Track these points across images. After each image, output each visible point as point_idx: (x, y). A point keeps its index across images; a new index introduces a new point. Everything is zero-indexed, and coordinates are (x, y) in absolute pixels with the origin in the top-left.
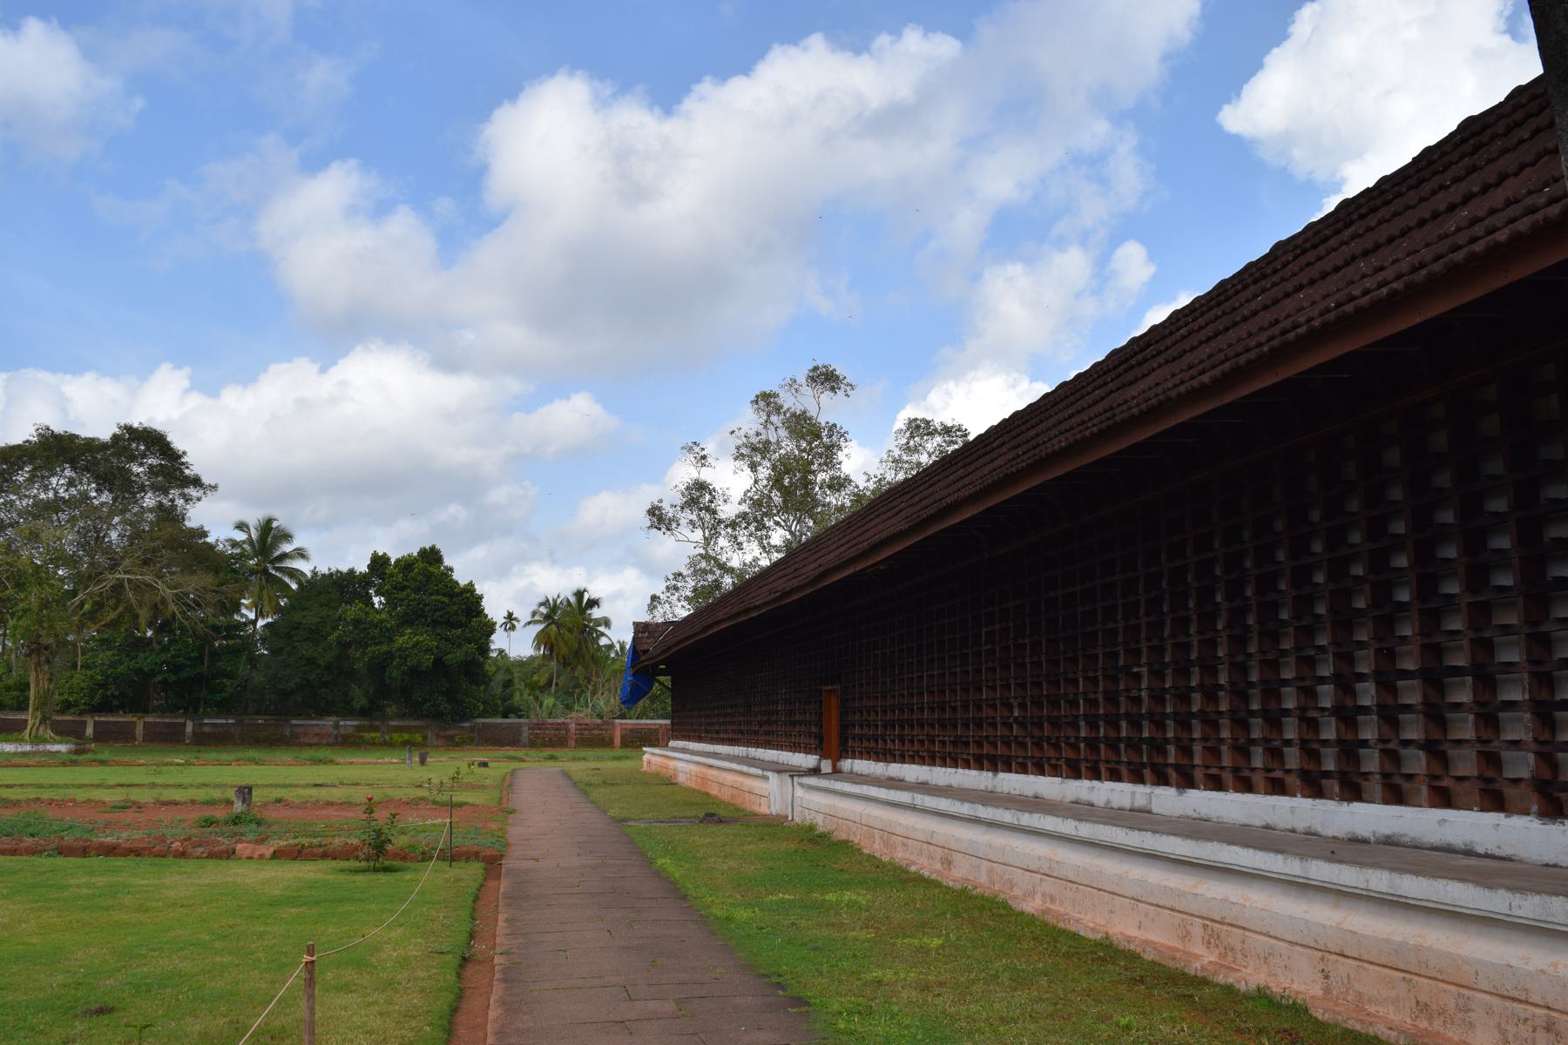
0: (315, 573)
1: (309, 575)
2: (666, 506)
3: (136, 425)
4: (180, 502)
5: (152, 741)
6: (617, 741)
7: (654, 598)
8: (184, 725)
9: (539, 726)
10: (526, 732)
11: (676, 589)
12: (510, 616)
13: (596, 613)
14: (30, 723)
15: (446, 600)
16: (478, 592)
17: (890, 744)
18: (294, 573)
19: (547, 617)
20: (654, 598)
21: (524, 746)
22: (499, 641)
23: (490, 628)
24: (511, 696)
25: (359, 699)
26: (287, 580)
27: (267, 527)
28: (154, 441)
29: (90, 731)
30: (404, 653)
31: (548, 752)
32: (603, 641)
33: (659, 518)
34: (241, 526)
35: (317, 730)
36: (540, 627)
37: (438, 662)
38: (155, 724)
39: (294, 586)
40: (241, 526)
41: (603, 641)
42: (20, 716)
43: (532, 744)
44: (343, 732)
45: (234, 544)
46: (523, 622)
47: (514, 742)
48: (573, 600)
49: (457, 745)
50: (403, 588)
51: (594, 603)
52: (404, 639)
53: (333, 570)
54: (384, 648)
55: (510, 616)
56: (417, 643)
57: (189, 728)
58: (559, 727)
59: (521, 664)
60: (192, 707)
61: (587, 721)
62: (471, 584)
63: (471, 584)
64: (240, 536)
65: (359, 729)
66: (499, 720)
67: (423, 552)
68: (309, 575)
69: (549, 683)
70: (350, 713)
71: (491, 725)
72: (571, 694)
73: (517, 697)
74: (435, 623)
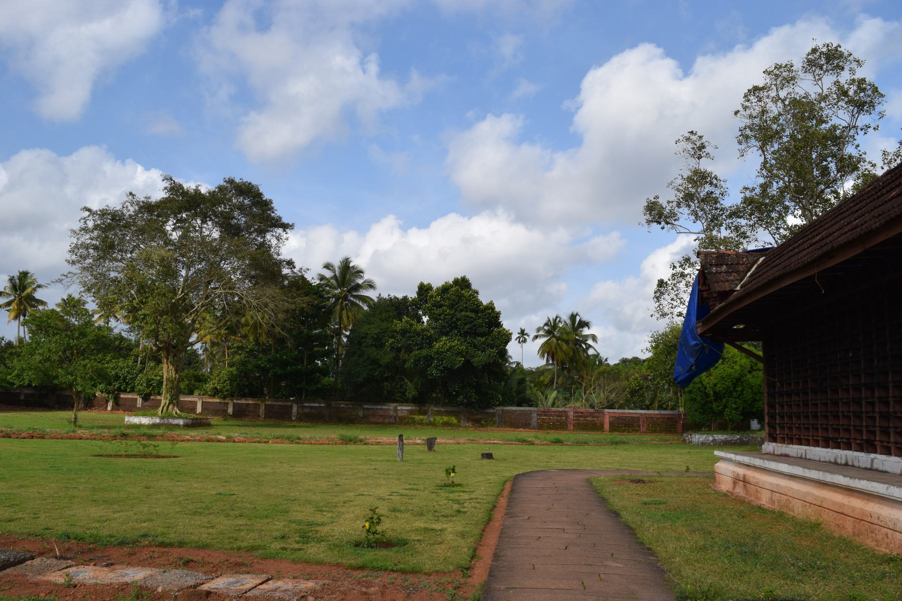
0: (380, 298)
1: (376, 300)
2: (662, 201)
3: (237, 180)
4: (274, 242)
5: (270, 417)
6: (607, 426)
7: (661, 283)
8: (291, 407)
9: (545, 413)
11: (683, 275)
12: (522, 332)
13: (586, 331)
14: (163, 402)
15: (473, 315)
16: (497, 310)
17: (794, 431)
18: (364, 299)
19: (549, 332)
20: (661, 283)
21: (534, 428)
22: (513, 349)
23: (507, 337)
24: (524, 390)
25: (411, 390)
26: (361, 304)
27: (346, 265)
28: (248, 190)
29: (230, 410)
30: (438, 358)
31: (553, 435)
32: (591, 352)
33: (657, 214)
34: (328, 266)
35: (381, 413)
36: (543, 340)
37: (468, 363)
38: (272, 406)
39: (366, 308)
40: (328, 266)
41: (591, 352)
42: (159, 397)
43: (540, 427)
44: (400, 414)
45: (322, 278)
46: (532, 336)
47: (526, 425)
49: (483, 426)
50: (441, 306)
51: (584, 324)
52: (442, 343)
53: (392, 295)
54: (424, 352)
55: (522, 332)
56: (450, 348)
57: (295, 410)
59: (530, 372)
61: (582, 410)
62: (491, 303)
63: (491, 303)
64: (328, 274)
65: (411, 412)
66: (514, 408)
67: (456, 282)
68: (376, 300)
69: (552, 381)
70: (406, 401)
71: (509, 412)
72: (569, 390)
73: (528, 392)
74: (465, 334)
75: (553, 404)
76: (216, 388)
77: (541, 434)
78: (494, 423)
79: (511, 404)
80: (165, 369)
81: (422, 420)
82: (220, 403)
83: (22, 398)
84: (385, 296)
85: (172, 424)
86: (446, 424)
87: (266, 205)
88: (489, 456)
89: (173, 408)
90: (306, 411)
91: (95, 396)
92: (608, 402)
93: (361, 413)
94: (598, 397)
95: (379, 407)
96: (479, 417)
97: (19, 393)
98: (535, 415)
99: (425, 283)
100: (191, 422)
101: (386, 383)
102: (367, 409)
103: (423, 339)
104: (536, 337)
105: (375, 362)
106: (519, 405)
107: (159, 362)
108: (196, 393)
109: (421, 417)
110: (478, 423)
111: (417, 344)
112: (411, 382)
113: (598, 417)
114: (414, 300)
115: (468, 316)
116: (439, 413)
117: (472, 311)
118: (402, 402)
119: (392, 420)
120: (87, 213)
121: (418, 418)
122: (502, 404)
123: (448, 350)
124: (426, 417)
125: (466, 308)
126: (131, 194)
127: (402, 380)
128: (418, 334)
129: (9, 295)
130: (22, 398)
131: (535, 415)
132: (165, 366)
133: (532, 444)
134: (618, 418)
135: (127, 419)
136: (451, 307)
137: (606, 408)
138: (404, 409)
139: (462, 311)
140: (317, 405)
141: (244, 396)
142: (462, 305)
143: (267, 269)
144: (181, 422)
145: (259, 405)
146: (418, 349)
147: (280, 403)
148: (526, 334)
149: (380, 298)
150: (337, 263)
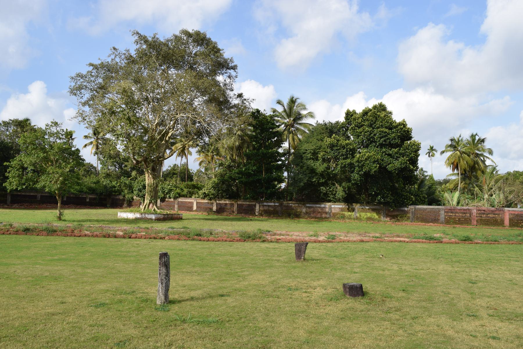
5: (241, 213)
6: (507, 222)
8: (255, 206)
9: (452, 210)
10: (442, 215)
12: (432, 149)
15: (387, 130)
21: (442, 223)
22: (423, 162)
25: (340, 191)
29: (215, 208)
36: (449, 154)
43: (447, 222)
44: (333, 211)
47: (435, 220)
48: (469, 139)
52: (363, 153)
56: (369, 157)
58: (465, 212)
60: (256, 198)
65: (342, 210)
70: (336, 201)
71: (420, 209)
74: (382, 146)
75: (458, 203)
76: (205, 193)
77: (448, 229)
78: (408, 218)
79: (423, 203)
80: (147, 178)
82: (208, 203)
83: (88, 200)
84: (321, 122)
85: (147, 219)
87: (216, 50)
89: (153, 207)
90: (266, 208)
91: (133, 199)
92: (507, 201)
93: (304, 210)
94: (498, 198)
95: (318, 206)
96: (396, 213)
97: (86, 198)
98: (442, 212)
99: (351, 110)
100: (162, 217)
101: (322, 188)
102: (309, 207)
103: (347, 151)
104: (443, 152)
105: (313, 171)
106: (430, 204)
107: (142, 173)
108: (193, 197)
109: (349, 213)
110: (393, 217)
111: (342, 155)
112: (340, 186)
113: (498, 215)
114: (343, 124)
115: (382, 132)
116: (363, 210)
117: (386, 128)
119: (328, 216)
120: (92, 68)
121: (347, 214)
122: (414, 204)
123: (366, 159)
124: (353, 213)
125: (382, 126)
126: (114, 49)
127: (334, 185)
128: (344, 147)
129: (91, 137)
130: (88, 200)
131: (442, 212)
132: (147, 175)
133: (439, 241)
134: (517, 215)
135: (119, 215)
136: (370, 126)
137: (506, 207)
138: (336, 207)
139: (378, 128)
140: (273, 204)
141: (222, 198)
142: (378, 123)
143: (219, 101)
144: (153, 217)
145: (233, 204)
146: (344, 159)
147: (248, 203)
148: (434, 150)
149: (318, 124)
150: (286, 102)
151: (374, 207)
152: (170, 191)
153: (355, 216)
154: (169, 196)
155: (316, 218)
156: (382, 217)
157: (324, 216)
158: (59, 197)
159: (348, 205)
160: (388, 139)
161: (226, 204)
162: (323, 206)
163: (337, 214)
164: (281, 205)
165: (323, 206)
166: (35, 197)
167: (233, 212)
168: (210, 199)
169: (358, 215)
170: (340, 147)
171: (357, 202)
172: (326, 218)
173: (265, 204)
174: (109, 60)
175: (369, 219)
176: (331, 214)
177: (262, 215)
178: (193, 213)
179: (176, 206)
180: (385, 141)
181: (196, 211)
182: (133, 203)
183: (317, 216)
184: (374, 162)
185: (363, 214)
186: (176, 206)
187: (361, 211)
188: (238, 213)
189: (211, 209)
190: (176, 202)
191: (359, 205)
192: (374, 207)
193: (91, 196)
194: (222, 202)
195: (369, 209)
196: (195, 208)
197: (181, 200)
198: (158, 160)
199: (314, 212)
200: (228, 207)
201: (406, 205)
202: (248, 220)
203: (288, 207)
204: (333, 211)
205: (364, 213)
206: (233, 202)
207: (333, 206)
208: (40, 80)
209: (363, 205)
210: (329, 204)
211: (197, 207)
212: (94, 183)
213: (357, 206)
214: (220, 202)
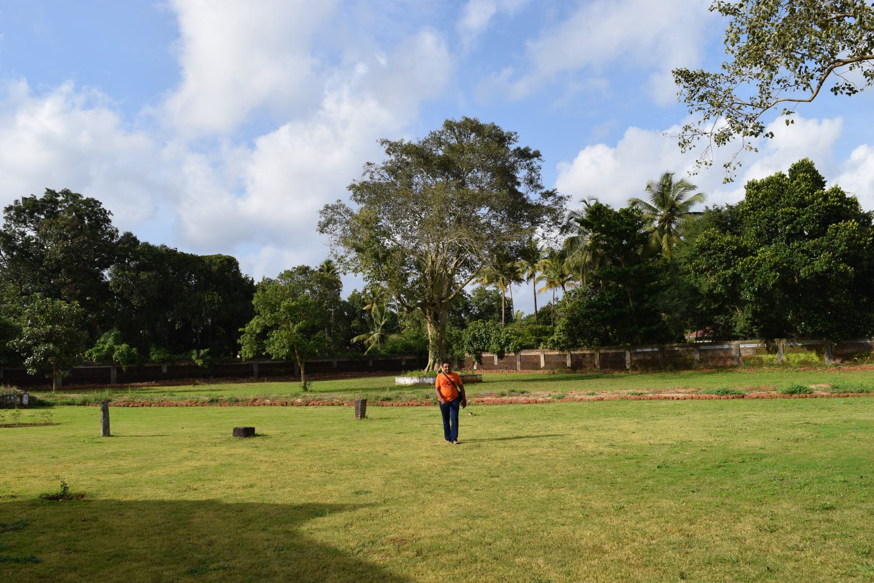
8: (624, 354)
44: (744, 354)
65: (757, 351)
81: (771, 360)
82: (560, 355)
83: (404, 363)
86: (805, 364)
88: (248, 432)
90: (640, 357)
105: (695, 291)
109: (770, 356)
110: (847, 358)
115: (786, 213)
116: (793, 349)
118: (745, 339)
119: (735, 363)
121: (766, 357)
124: (776, 356)
126: (369, 164)
138: (748, 347)
140: (648, 350)
146: (724, 269)
149: (709, 212)
151: (810, 343)
152: (508, 341)
153: (779, 361)
154: (508, 349)
155: (716, 367)
156: (826, 359)
157: (729, 363)
158: (301, 363)
159: (766, 342)
160: (797, 224)
161: (584, 355)
162: (726, 346)
163: (751, 359)
164: (662, 350)
165: (726, 346)
166: (330, 364)
167: (595, 366)
168: (562, 349)
169: (784, 358)
170: (715, 249)
171: (781, 336)
172: (732, 366)
173: (638, 350)
174: (367, 178)
175: (805, 364)
176: (740, 359)
177: (636, 369)
178: (540, 372)
179: (518, 363)
180: (794, 228)
181: (545, 368)
182: (465, 364)
183: (719, 365)
184: (771, 269)
185: (792, 356)
186: (518, 363)
187: (789, 352)
188: (601, 368)
189: (565, 364)
190: (518, 357)
191: (784, 341)
192: (810, 343)
193: (408, 358)
194: (578, 352)
195: (802, 347)
196: (543, 364)
197: (524, 353)
198: (440, 302)
199: (713, 358)
200: (588, 359)
201: (863, 336)
202: (613, 377)
203: (673, 353)
204: (744, 354)
205: (794, 355)
206: (593, 351)
207: (742, 346)
208: (583, 148)
209: (792, 341)
210: (736, 342)
211: (546, 363)
212: (413, 338)
213: (782, 343)
214: (576, 353)
